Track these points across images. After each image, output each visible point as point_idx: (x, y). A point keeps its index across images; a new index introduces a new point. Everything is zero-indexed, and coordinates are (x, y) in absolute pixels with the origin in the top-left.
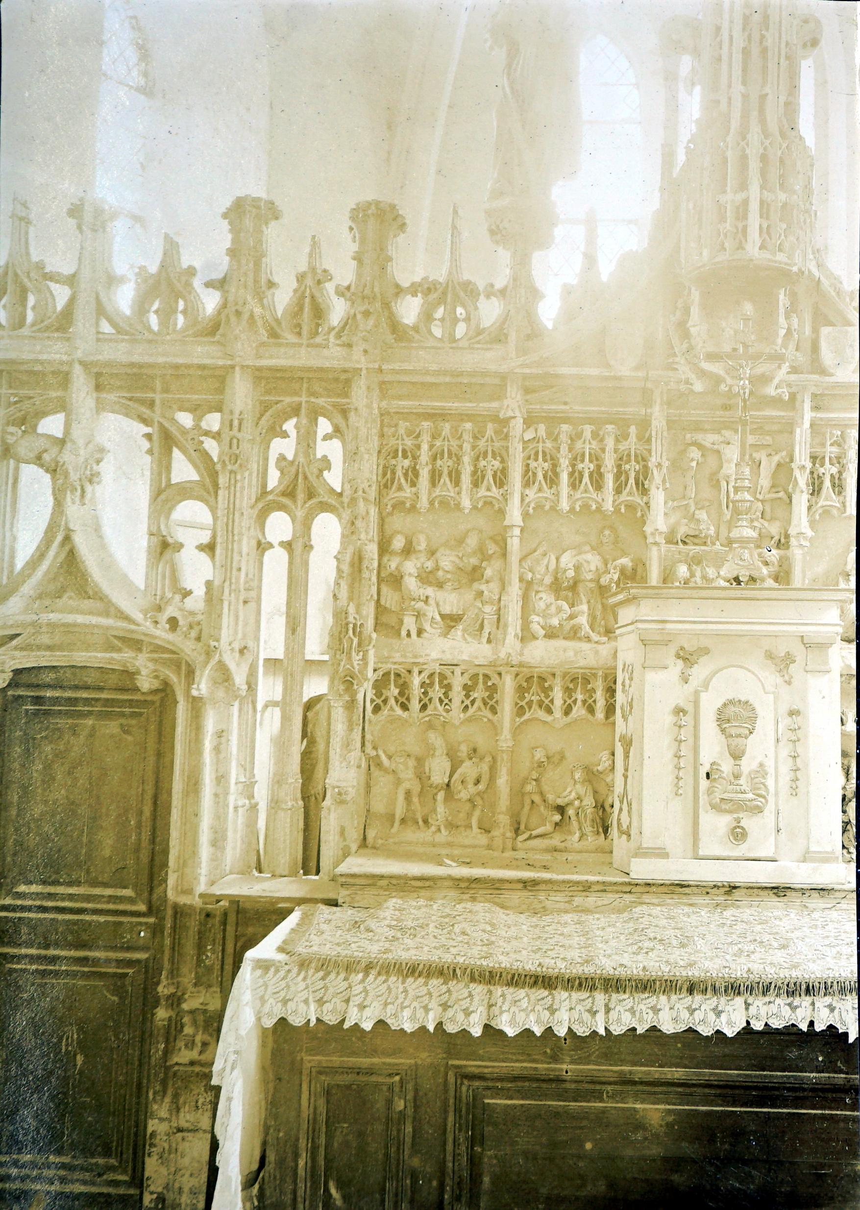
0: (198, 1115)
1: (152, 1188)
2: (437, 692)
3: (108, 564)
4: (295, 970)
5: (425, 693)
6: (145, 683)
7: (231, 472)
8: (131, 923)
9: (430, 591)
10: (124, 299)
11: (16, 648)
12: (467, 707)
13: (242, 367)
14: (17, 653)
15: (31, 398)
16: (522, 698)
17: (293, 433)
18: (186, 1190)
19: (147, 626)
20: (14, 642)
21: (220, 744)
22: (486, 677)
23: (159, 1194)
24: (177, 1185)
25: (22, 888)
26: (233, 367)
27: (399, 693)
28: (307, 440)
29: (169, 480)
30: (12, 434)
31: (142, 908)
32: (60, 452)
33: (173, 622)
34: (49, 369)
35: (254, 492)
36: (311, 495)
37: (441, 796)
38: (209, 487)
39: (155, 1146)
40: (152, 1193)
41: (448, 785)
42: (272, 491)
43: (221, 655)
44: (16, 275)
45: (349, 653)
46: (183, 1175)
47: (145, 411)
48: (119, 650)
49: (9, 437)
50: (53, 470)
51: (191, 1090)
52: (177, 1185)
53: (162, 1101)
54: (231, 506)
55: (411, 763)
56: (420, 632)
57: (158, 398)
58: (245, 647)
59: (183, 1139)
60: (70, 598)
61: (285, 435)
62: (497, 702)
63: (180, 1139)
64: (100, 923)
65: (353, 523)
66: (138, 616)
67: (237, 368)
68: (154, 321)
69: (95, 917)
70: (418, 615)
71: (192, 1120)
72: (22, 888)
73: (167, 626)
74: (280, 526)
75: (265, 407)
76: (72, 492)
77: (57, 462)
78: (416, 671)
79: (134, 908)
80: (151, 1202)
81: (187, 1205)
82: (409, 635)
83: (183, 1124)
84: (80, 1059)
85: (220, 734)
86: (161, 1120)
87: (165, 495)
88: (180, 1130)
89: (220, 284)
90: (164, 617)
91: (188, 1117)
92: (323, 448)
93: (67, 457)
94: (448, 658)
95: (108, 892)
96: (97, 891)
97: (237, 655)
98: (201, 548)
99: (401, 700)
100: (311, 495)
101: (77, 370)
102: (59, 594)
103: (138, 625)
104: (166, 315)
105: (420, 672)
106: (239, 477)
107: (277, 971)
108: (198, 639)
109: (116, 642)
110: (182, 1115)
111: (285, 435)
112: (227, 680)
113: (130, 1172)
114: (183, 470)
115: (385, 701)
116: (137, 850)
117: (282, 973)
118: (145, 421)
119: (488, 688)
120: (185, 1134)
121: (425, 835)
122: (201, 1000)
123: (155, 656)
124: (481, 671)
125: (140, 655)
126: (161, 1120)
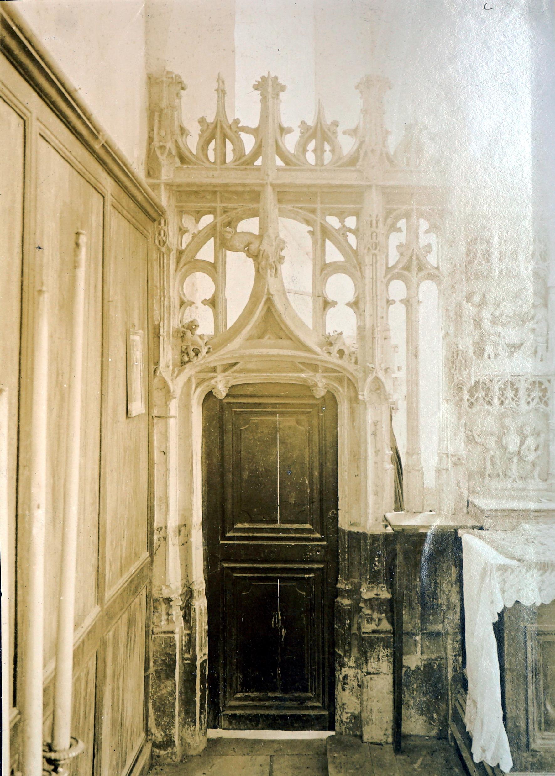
0: (380, 664)
1: (346, 710)
2: (510, 393)
3: (295, 317)
4: (524, 571)
5: (503, 395)
6: (320, 392)
7: (373, 255)
8: (312, 545)
9: (500, 329)
10: (290, 143)
11: (236, 372)
12: (529, 403)
13: (377, 186)
14: (238, 375)
15: (236, 209)
16: (529, 395)
17: (404, 229)
18: (375, 710)
19: (324, 356)
20: (235, 368)
21: (376, 429)
22: (540, 383)
23: (352, 713)
24: (369, 708)
25: (239, 526)
26: (370, 187)
27: (486, 395)
28: (413, 232)
29: (325, 261)
30: (229, 232)
31: (318, 535)
32: (261, 243)
33: (341, 353)
34: (248, 189)
35: (384, 267)
36: (420, 269)
37: (515, 459)
38: (353, 265)
39: (347, 684)
40: (347, 713)
41: (519, 452)
42: (394, 267)
43: (376, 372)
44: (222, 128)
45: (460, 370)
46: (372, 701)
47: (310, 216)
48: (302, 371)
49: (227, 234)
50: (256, 256)
51: (375, 649)
52: (369, 708)
53: (350, 656)
54: (375, 277)
55: (494, 439)
56: (496, 355)
57: (319, 206)
58: (388, 368)
59: (371, 679)
60: (269, 338)
61: (400, 230)
62: (548, 399)
63: (369, 679)
64: (292, 546)
65: (453, 286)
66: (318, 349)
67: (374, 188)
68: (311, 158)
69: (287, 543)
70: (495, 345)
71: (376, 667)
72: (239, 526)
73: (338, 355)
74: (397, 289)
75: (389, 213)
76: (270, 269)
77: (259, 251)
78: (496, 380)
79: (312, 536)
80: (347, 718)
81: (376, 719)
82: (489, 357)
83: (371, 670)
84: (284, 632)
85: (375, 424)
86: (351, 667)
87: (324, 270)
88: (368, 673)
89: (354, 132)
90: (334, 350)
91: (374, 665)
92: (424, 240)
93: (265, 246)
94: (517, 371)
95: (295, 526)
96: (288, 526)
97: (384, 372)
98: (349, 304)
99: (487, 399)
100: (420, 269)
101: (269, 189)
102: (261, 337)
103: (318, 355)
104: (319, 151)
105: (499, 381)
106: (378, 258)
107: (513, 571)
108: (356, 363)
109: (301, 366)
110: (369, 664)
111: (400, 230)
112: (378, 389)
113: (321, 702)
114: (333, 254)
115: (476, 400)
116: (311, 497)
117: (516, 573)
118: (308, 223)
119: (542, 390)
120: (372, 676)
121: (508, 484)
122: (375, 592)
123: (326, 374)
124: (538, 379)
125: (317, 375)
126: (351, 667)
